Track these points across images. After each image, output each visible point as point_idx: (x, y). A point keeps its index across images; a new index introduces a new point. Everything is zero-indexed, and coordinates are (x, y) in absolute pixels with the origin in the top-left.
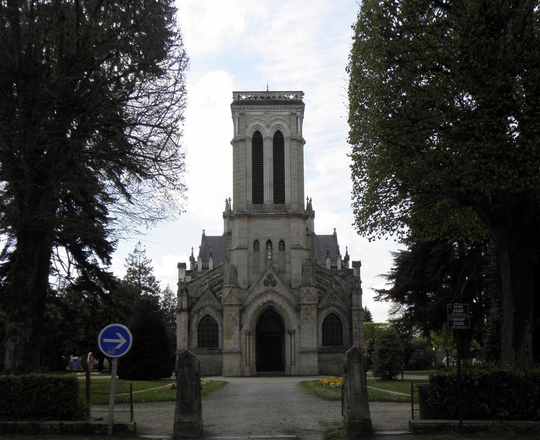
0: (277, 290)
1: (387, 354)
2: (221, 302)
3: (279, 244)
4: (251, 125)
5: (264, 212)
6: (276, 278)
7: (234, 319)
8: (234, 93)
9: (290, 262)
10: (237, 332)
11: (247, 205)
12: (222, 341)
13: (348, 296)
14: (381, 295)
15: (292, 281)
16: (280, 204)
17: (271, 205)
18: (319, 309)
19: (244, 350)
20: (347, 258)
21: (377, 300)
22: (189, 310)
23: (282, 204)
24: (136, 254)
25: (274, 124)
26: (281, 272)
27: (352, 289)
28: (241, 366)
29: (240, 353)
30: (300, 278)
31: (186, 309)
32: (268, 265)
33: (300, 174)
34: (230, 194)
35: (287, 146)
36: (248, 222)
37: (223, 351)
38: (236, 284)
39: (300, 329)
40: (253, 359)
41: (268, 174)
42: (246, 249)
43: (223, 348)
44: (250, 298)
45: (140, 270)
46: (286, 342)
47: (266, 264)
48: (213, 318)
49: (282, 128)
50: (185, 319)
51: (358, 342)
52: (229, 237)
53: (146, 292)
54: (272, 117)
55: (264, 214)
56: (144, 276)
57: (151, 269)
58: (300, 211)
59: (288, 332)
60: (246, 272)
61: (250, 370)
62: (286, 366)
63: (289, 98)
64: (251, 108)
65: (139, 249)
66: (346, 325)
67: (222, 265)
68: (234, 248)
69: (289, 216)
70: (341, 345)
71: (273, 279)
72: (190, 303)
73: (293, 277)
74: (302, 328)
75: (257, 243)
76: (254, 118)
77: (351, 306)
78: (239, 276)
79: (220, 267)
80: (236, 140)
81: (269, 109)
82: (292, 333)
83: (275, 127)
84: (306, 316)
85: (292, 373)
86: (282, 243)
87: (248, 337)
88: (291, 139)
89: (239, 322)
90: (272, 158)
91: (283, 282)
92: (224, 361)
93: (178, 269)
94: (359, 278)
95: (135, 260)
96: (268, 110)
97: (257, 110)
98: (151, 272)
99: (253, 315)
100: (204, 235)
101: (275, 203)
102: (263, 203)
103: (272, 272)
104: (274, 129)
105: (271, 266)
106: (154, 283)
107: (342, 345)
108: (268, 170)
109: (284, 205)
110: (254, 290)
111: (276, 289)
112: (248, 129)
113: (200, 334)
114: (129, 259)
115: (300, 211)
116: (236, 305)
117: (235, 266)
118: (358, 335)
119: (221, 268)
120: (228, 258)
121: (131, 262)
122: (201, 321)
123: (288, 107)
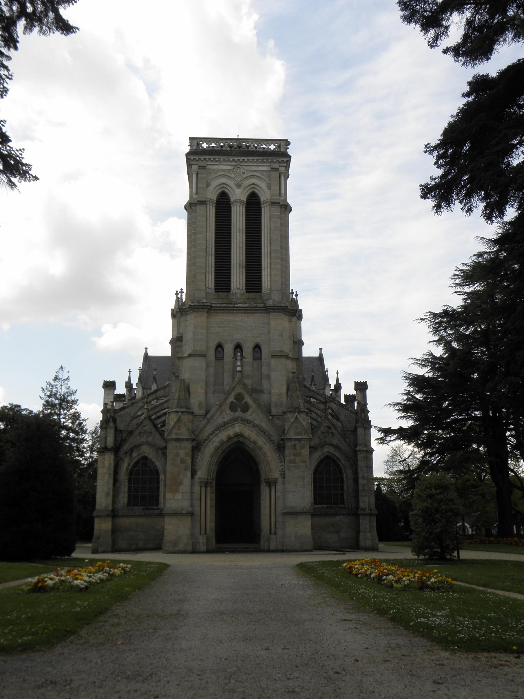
0: (249, 418)
1: (438, 516)
3: (253, 350)
4: (215, 183)
5: (231, 304)
6: (248, 399)
7: (182, 461)
8: (191, 139)
9: (268, 377)
10: (187, 481)
11: (207, 293)
12: (164, 497)
14: (386, 436)
15: (272, 404)
16: (255, 294)
17: (242, 294)
19: (197, 510)
20: (338, 386)
21: (381, 443)
22: (116, 449)
23: (257, 294)
24: (56, 383)
25: (247, 183)
26: (256, 391)
27: (357, 421)
29: (192, 514)
31: (112, 448)
32: (237, 379)
34: (182, 283)
35: (266, 213)
36: (207, 318)
37: (163, 512)
38: (188, 408)
39: (284, 478)
40: (211, 525)
41: (238, 251)
42: (204, 356)
43: (164, 507)
44: (209, 429)
45: (60, 404)
46: (263, 497)
47: (233, 379)
48: (153, 463)
49: (258, 188)
50: (110, 464)
52: (179, 343)
53: (68, 433)
54: (244, 173)
55: (231, 306)
57: (74, 402)
58: (285, 303)
59: (266, 482)
60: (204, 391)
61: (205, 541)
62: (262, 535)
63: (268, 149)
64: (215, 159)
66: (348, 473)
67: (168, 385)
68: (186, 355)
69: (268, 309)
71: (243, 402)
72: (119, 439)
73: (274, 399)
74: (286, 476)
75: (220, 349)
76: (219, 174)
77: (356, 445)
78: (192, 396)
79: (165, 387)
80: (192, 202)
81: (241, 162)
82: (271, 483)
83: (249, 187)
84: (293, 457)
85: (272, 547)
86: (256, 349)
87: (203, 489)
88: (272, 203)
89: (190, 465)
91: (259, 406)
92: (166, 527)
93: (103, 390)
94: (366, 405)
95: (54, 390)
96: (239, 163)
97: (224, 164)
98: (75, 406)
99: (212, 456)
100: (146, 355)
101: (247, 292)
102: (230, 292)
103: (243, 391)
105: (241, 382)
106: (78, 421)
107: (343, 503)
108: (238, 245)
109: (261, 295)
110: (215, 418)
111: (248, 415)
112: (211, 188)
114: (47, 389)
115: (285, 303)
116: (187, 440)
117: (186, 381)
118: (366, 488)
119: (167, 389)
120: (177, 374)
121: (48, 393)
122: (135, 466)
123: (267, 160)
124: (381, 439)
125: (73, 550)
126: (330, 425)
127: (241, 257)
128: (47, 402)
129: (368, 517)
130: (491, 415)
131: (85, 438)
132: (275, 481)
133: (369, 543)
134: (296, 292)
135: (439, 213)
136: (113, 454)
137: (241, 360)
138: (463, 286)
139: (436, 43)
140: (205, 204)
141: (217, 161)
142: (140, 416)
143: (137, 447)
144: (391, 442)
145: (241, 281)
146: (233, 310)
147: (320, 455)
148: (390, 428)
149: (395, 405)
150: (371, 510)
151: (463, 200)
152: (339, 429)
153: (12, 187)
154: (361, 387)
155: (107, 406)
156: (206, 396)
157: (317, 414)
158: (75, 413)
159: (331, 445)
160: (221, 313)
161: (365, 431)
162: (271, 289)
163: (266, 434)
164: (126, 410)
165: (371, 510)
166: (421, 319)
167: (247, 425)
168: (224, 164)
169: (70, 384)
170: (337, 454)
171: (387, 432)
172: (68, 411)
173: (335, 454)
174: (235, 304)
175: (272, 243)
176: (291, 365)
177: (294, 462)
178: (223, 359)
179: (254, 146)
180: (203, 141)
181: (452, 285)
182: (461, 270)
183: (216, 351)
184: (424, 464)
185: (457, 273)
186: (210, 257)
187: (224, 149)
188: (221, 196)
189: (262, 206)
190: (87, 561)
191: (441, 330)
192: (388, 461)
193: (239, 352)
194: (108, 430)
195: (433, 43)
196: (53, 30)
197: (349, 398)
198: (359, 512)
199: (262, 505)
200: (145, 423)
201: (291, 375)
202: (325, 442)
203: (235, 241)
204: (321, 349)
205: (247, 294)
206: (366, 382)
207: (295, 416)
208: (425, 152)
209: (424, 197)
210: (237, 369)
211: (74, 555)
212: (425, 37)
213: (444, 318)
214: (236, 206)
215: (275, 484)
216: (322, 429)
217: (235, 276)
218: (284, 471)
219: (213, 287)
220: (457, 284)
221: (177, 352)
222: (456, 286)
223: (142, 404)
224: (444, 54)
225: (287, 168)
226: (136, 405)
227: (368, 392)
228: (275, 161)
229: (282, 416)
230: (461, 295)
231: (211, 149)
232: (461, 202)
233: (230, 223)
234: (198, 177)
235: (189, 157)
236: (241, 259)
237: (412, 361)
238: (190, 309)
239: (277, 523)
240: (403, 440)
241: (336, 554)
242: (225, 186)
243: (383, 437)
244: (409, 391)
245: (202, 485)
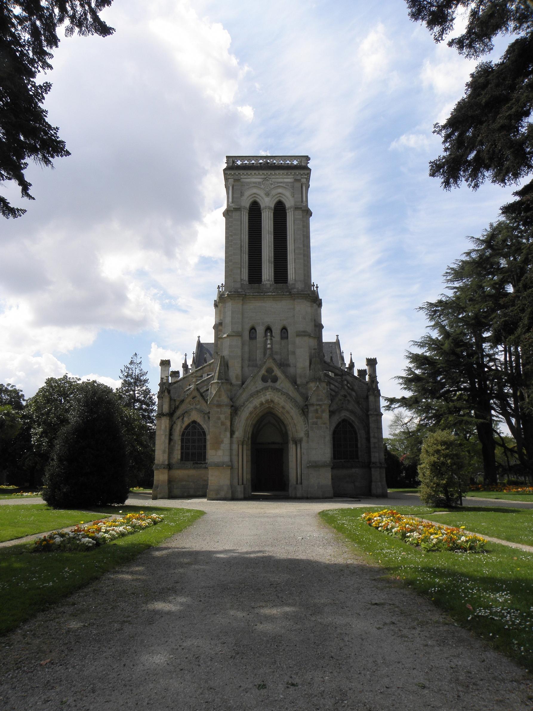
0: (278, 387)
3: (281, 331)
5: (262, 293)
6: (277, 372)
7: (223, 424)
9: (294, 353)
11: (242, 284)
14: (391, 404)
16: (281, 285)
19: (235, 464)
20: (352, 365)
21: (387, 410)
23: (284, 284)
24: (132, 366)
25: (274, 192)
26: (283, 365)
27: (368, 390)
28: (232, 486)
30: (308, 372)
36: (243, 305)
39: (308, 437)
40: (247, 476)
41: (267, 248)
44: (244, 396)
45: (135, 383)
47: (265, 354)
48: (199, 425)
50: (166, 427)
51: (377, 455)
52: (220, 328)
56: (139, 388)
57: (146, 381)
58: (307, 291)
59: (293, 441)
60: (240, 365)
61: (243, 490)
62: (290, 485)
63: (292, 164)
65: (135, 360)
66: (361, 434)
72: (173, 407)
75: (253, 330)
76: (251, 185)
78: (231, 369)
82: (297, 442)
83: (276, 196)
84: (315, 420)
85: (299, 495)
86: (284, 330)
87: (240, 447)
91: (287, 377)
92: (210, 478)
97: (255, 177)
101: (275, 283)
102: (261, 283)
104: (274, 198)
108: (267, 244)
112: (245, 198)
113: (184, 444)
115: (307, 291)
117: (225, 357)
118: (377, 445)
121: (126, 374)
124: (387, 406)
125: (126, 498)
126: (346, 393)
127: (270, 255)
128: (125, 381)
130: (477, 386)
131: (154, 409)
133: (379, 491)
134: (317, 285)
135: (447, 188)
136: (168, 418)
137: (271, 339)
138: (453, 281)
139: (442, 38)
141: (249, 175)
144: (395, 409)
145: (270, 274)
148: (394, 398)
149: (399, 378)
150: (381, 464)
151: (469, 178)
152: (354, 398)
153: (46, 164)
154: (372, 363)
156: (242, 370)
157: (335, 386)
158: (146, 390)
162: (295, 280)
164: (178, 383)
165: (381, 464)
166: (420, 308)
168: (255, 177)
169: (142, 367)
170: (352, 418)
171: (392, 401)
172: (141, 388)
173: (351, 417)
174: (265, 293)
176: (313, 342)
177: (316, 423)
181: (444, 281)
182: (451, 269)
183: (250, 333)
184: (420, 427)
185: (449, 271)
186: (245, 255)
189: (287, 211)
190: (82, 522)
191: (436, 317)
192: (391, 425)
193: (269, 332)
194: (164, 400)
195: (439, 38)
196: (92, 32)
197: (362, 373)
198: (371, 466)
199: (290, 460)
201: (313, 351)
202: (342, 407)
204: (337, 336)
205: (275, 284)
206: (376, 358)
208: (434, 132)
209: (433, 175)
211: (129, 502)
212: (431, 32)
213: (439, 307)
215: (301, 442)
217: (265, 270)
218: (308, 431)
219: (247, 279)
220: (449, 280)
222: (447, 282)
224: (449, 47)
227: (377, 366)
228: (297, 173)
230: (452, 289)
231: (245, 165)
232: (467, 180)
233: (261, 226)
235: (226, 172)
236: (270, 256)
237: (412, 343)
240: (405, 407)
241: (352, 501)
242: (256, 196)
243: (389, 405)
244: (410, 368)
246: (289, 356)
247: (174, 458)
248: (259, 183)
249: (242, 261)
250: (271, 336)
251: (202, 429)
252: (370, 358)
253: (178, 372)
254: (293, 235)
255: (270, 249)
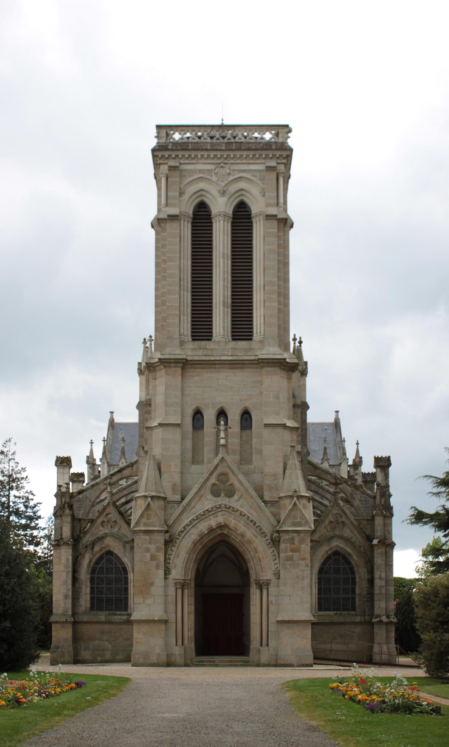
2: (128, 523)
7: (153, 558)
8: (159, 127)
9: (260, 452)
13: (367, 520)
15: (265, 487)
18: (316, 541)
19: (172, 618)
28: (167, 645)
33: (282, 250)
41: (222, 283)
48: (117, 557)
50: (68, 559)
51: (383, 605)
54: (229, 174)
59: (256, 584)
60: (178, 470)
63: (262, 138)
67: (136, 462)
70: (352, 610)
74: (282, 576)
75: (198, 415)
76: (196, 177)
81: (226, 159)
83: (237, 195)
84: (290, 554)
86: (246, 416)
87: (179, 591)
88: (267, 216)
89: (163, 563)
90: (230, 253)
93: (55, 468)
96: (222, 160)
97: (202, 161)
104: (233, 198)
108: (222, 275)
110: (193, 504)
111: (233, 502)
112: (186, 197)
113: (95, 586)
119: (135, 467)
122: (97, 563)
127: (226, 293)
129: (384, 626)
132: (267, 582)
134: (300, 338)
137: (226, 430)
140: (178, 220)
142: (103, 501)
143: (101, 539)
145: (226, 325)
146: (215, 364)
147: (326, 550)
155: (62, 488)
156: (182, 477)
159: (341, 537)
160: (200, 368)
161: (384, 520)
162: (264, 335)
163: (257, 525)
164: (84, 493)
167: (233, 513)
175: (266, 271)
177: (290, 559)
178: (203, 429)
179: (243, 135)
180: (175, 130)
186: (186, 293)
187: (202, 140)
188: (199, 208)
199: (252, 611)
200: (108, 511)
203: (218, 270)
204: (337, 412)
206: (389, 457)
207: (294, 502)
210: (220, 441)
214: (219, 221)
215: (268, 586)
216: (331, 518)
217: (218, 318)
218: (279, 571)
219: (189, 333)
221: (147, 420)
223: (105, 486)
225: (288, 166)
226: (96, 487)
229: (277, 501)
234: (169, 182)
235: (156, 153)
236: (226, 294)
238: (159, 363)
239: (269, 633)
245: (177, 587)
246: (253, 456)
247: (81, 606)
248: (209, 171)
249: (182, 304)
250: (226, 424)
251: (122, 563)
252: (380, 456)
253: (82, 475)
254: (262, 260)
255: (226, 284)
